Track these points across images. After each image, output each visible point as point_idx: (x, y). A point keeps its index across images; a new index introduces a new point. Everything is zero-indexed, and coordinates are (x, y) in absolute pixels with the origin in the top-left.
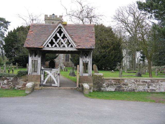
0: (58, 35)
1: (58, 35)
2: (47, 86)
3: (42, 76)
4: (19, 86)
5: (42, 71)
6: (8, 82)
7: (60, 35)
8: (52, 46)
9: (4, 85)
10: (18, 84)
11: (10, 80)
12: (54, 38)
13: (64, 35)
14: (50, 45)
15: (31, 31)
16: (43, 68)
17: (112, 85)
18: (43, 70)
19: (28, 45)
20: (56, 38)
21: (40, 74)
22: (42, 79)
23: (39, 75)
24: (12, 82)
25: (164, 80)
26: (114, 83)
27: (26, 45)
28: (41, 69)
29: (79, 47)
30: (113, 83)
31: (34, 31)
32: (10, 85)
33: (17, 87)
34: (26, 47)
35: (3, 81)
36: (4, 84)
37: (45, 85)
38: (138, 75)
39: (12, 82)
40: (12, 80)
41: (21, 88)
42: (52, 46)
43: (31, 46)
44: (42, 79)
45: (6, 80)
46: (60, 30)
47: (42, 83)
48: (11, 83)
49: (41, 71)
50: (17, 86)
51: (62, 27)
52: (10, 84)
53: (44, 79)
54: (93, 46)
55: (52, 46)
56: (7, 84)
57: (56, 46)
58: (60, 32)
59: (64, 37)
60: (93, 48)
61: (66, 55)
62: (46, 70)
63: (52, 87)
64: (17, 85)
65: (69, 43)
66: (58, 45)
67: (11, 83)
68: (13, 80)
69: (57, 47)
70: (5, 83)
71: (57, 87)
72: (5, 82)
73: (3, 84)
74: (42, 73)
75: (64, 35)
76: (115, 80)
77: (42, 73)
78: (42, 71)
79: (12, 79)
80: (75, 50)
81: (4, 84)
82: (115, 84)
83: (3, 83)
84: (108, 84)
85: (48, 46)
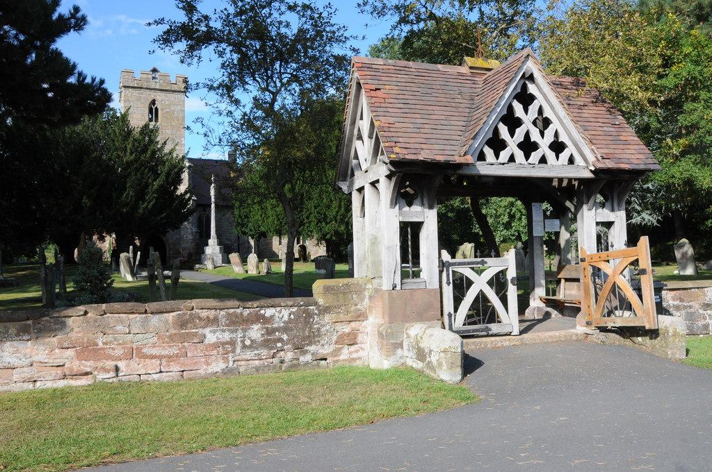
0: (504, 131)
1: (504, 131)
2: (473, 337)
3: (448, 292)
5: (448, 271)
6: (270, 332)
7: (512, 134)
9: (250, 347)
10: (313, 337)
14: (489, 152)
15: (374, 87)
19: (405, 151)
20: (512, 122)
24: (285, 329)
26: (676, 303)
28: (443, 265)
29: (609, 164)
31: (387, 91)
32: (279, 345)
35: (244, 330)
36: (248, 342)
39: (285, 329)
40: (284, 322)
46: (524, 87)
49: (441, 272)
50: (312, 348)
51: (537, 75)
52: (280, 340)
56: (267, 344)
58: (525, 99)
60: (652, 167)
61: (283, 286)
64: (310, 344)
65: (558, 147)
66: (520, 155)
67: (285, 337)
71: (509, 334)
72: (256, 332)
73: (244, 347)
76: (675, 292)
78: (448, 271)
79: (286, 318)
81: (248, 342)
83: (243, 342)
85: (482, 157)
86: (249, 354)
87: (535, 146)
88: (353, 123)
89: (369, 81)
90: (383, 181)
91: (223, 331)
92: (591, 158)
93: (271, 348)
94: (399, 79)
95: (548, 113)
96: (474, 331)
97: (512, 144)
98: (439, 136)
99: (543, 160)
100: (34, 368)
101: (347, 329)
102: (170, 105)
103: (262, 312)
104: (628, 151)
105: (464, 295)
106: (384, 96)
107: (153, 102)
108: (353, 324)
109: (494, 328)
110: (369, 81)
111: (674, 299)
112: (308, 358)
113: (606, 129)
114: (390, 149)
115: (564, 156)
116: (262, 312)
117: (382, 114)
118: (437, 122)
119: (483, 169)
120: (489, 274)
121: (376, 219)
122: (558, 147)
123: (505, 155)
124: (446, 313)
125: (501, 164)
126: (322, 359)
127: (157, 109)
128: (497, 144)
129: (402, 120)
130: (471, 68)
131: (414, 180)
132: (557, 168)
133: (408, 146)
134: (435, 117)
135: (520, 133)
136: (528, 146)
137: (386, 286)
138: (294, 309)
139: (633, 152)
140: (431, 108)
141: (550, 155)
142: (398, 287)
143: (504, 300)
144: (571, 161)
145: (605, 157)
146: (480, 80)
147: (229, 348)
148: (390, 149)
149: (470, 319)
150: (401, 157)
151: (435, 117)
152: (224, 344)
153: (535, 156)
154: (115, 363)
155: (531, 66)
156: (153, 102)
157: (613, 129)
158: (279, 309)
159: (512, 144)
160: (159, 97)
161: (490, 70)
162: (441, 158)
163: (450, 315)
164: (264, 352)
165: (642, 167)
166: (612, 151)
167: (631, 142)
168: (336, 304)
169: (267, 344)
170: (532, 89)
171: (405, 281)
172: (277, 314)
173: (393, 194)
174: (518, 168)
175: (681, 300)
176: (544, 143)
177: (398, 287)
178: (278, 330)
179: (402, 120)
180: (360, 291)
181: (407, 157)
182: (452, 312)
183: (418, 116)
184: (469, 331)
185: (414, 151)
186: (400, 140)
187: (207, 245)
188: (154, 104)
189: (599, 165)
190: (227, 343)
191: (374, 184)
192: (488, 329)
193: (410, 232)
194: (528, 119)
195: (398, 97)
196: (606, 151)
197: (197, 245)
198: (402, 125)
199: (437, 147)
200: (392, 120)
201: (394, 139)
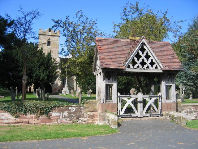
0: (140, 53)
1: (140, 53)
2: (125, 117)
3: (119, 104)
4: (83, 118)
5: (119, 98)
6: (70, 114)
8: (133, 66)
9: (64, 117)
10: (82, 116)
11: (72, 111)
12: (136, 56)
13: (147, 53)
15: (100, 46)
16: (119, 94)
17: (191, 112)
18: (119, 97)
19: (106, 65)
20: (138, 56)
21: (116, 103)
22: (119, 109)
23: (115, 104)
24: (74, 113)
25: (197, 104)
26: (194, 110)
27: (103, 65)
28: (118, 97)
29: (167, 69)
30: (193, 110)
31: (104, 48)
32: (72, 117)
33: (82, 120)
34: (103, 67)
35: (63, 113)
37: (124, 116)
38: (182, 102)
41: (87, 121)
42: (143, 66)
43: (111, 66)
44: (119, 109)
45: (67, 112)
46: (142, 47)
47: (120, 114)
48: (74, 115)
49: (117, 99)
51: (146, 43)
52: (73, 116)
53: (122, 109)
54: (181, 68)
55: (143, 66)
56: (69, 117)
57: (138, 67)
58: (143, 50)
59: (148, 57)
62: (123, 97)
63: (132, 118)
64: (81, 117)
65: (152, 63)
66: (140, 66)
67: (74, 115)
68: (75, 111)
69: (130, 67)
70: (65, 115)
71: (137, 117)
72: (66, 113)
73: (63, 117)
74: (119, 101)
75: (147, 53)
76: (194, 107)
77: (119, 101)
78: (119, 98)
80: (161, 71)
81: (64, 116)
82: (195, 112)
83: (62, 116)
84: (188, 112)
85: (129, 66)
86: (64, 120)
87: (145, 63)
88: (97, 55)
89: (99, 45)
90: (102, 73)
91: (57, 113)
92: (162, 67)
93: (70, 118)
94: (108, 44)
95: (149, 54)
96: (126, 116)
97: (138, 63)
98: (117, 61)
99: (148, 67)
100: (8, 120)
101: (91, 114)
102: (54, 40)
103: (68, 108)
104: (175, 65)
105: (146, 105)
106: (103, 49)
107: (49, 39)
108: (93, 112)
109: (133, 115)
110: (99, 45)
111: (193, 109)
112: (80, 121)
113: (170, 58)
114: (102, 65)
115: (154, 66)
116: (68, 108)
117: (101, 54)
118: (117, 57)
119: (128, 70)
120: (132, 99)
121: (101, 83)
122: (152, 63)
123: (136, 66)
124: (119, 110)
125: (134, 69)
126: (84, 122)
127: (50, 42)
128: (134, 63)
129: (106, 56)
130: (130, 40)
131: (109, 73)
132: (152, 70)
133: (107, 64)
134: (117, 55)
135: (141, 60)
136: (143, 63)
137: (102, 102)
138: (77, 108)
139: (176, 65)
140: (116, 52)
141: (150, 66)
142: (105, 103)
143: (137, 109)
144: (156, 67)
145: (166, 66)
146: (132, 43)
147: (58, 117)
148: (102, 65)
149: (126, 112)
150: (105, 67)
151: (117, 55)
152: (57, 116)
153: (145, 66)
154: (28, 120)
155: (144, 41)
156: (49, 39)
157: (171, 58)
158: (72, 108)
159: (138, 63)
160: (51, 38)
161: (136, 40)
162: (116, 67)
163: (119, 111)
164: (68, 119)
165: (178, 69)
166: (169, 65)
167: (176, 62)
168: (89, 106)
169: (69, 117)
170: (145, 47)
171: (107, 101)
172: (72, 109)
173: (103, 77)
174: (140, 70)
175: (196, 109)
176: (148, 63)
177: (105, 103)
178: (71, 113)
179: (106, 56)
180: (96, 103)
181: (106, 67)
182: (120, 110)
183: (112, 55)
184: (125, 116)
185: (108, 65)
186: (105, 62)
187: (64, 87)
188: (49, 40)
189: (164, 69)
190: (58, 116)
191: (100, 73)
192: (131, 115)
193: (108, 87)
194: (143, 56)
195: (107, 49)
196: (167, 65)
197: (62, 87)
198: (107, 58)
199: (115, 64)
200: (103, 56)
201: (104, 62)
